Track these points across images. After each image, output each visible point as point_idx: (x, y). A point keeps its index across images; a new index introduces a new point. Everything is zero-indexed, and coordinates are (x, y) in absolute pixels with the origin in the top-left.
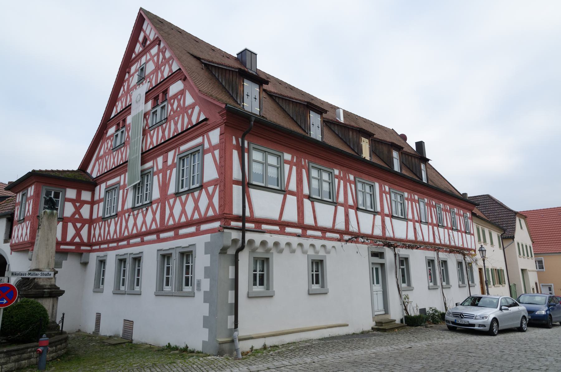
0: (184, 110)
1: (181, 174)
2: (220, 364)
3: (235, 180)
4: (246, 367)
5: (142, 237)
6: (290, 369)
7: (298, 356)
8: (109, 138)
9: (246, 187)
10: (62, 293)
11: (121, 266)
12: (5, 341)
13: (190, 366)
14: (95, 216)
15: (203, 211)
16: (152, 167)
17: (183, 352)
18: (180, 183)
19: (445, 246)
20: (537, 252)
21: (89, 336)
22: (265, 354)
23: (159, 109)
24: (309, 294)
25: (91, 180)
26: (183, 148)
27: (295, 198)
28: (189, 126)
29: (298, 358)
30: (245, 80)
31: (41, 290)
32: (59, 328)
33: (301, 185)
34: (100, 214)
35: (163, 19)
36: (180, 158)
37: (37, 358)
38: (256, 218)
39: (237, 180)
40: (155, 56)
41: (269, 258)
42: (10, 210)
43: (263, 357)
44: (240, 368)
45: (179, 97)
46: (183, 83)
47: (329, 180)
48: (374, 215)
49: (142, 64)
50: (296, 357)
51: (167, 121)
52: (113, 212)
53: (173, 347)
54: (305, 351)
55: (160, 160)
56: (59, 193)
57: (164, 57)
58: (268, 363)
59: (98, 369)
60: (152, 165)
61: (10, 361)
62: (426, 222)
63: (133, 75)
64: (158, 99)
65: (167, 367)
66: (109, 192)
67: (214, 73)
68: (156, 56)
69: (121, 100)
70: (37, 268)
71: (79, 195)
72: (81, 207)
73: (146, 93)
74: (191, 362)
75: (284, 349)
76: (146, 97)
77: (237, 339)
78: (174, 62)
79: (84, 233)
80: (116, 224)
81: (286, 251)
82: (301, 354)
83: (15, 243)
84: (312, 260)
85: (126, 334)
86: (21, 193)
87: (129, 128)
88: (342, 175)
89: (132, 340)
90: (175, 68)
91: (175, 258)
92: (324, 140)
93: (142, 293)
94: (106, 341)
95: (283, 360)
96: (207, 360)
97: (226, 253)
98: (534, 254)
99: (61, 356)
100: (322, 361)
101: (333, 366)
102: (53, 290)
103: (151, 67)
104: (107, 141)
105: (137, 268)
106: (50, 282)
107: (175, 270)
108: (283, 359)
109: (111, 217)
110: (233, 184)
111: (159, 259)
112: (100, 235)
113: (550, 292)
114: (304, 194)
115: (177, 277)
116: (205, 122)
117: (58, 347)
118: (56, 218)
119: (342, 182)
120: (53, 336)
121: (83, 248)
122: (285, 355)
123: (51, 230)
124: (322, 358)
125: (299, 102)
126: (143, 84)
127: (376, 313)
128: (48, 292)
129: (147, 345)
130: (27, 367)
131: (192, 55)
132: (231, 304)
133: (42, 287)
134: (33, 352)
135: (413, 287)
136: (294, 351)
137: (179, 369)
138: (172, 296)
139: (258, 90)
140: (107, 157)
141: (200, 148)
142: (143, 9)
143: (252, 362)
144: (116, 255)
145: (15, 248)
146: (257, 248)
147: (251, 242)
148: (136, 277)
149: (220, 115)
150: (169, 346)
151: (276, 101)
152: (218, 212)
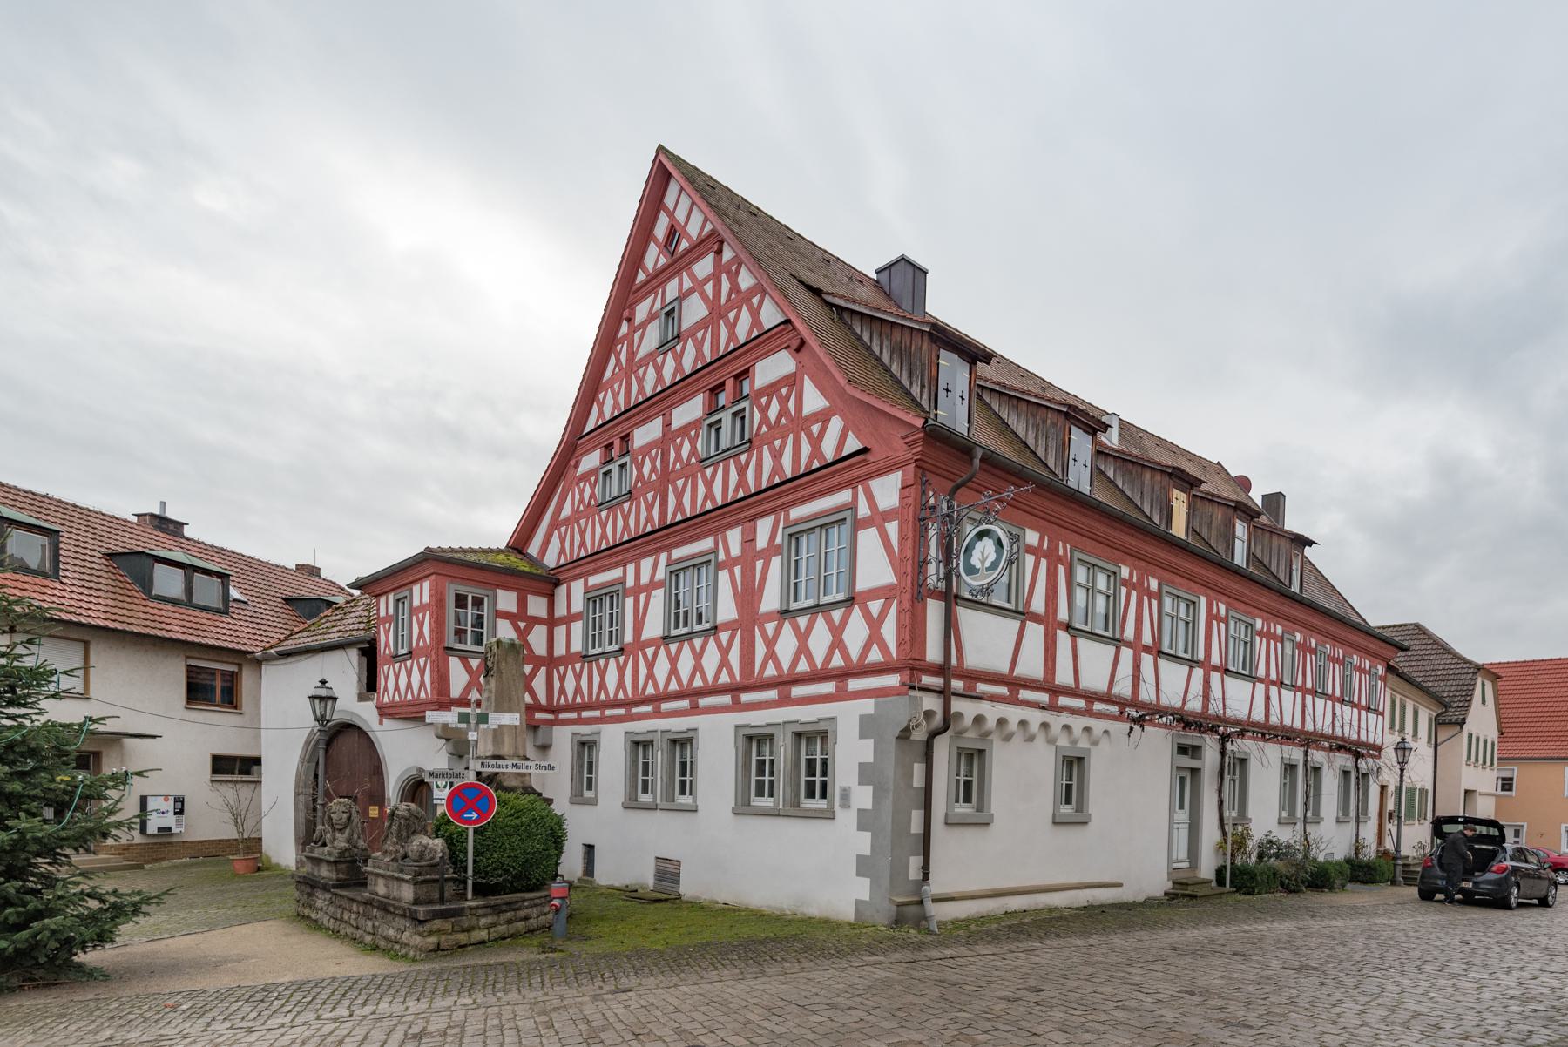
0: (800, 424)
11: (675, 754)
14: (560, 650)
18: (791, 589)
19: (1327, 737)
20: (1505, 756)
26: (796, 513)
27: (1040, 628)
40: (706, 281)
41: (984, 750)
45: (784, 391)
46: (795, 359)
47: (1108, 588)
48: (1191, 667)
52: (403, 648)
55: (734, 537)
57: (735, 287)
62: (1292, 686)
69: (612, 387)
70: (497, 753)
71: (522, 604)
72: (528, 630)
78: (767, 301)
81: (1018, 740)
90: (770, 316)
98: (1499, 759)
103: (695, 310)
104: (578, 484)
113: (1517, 839)
116: (861, 457)
119: (1134, 594)
121: (538, 716)
127: (1175, 866)
135: (1322, 819)
138: (779, 816)
141: (847, 514)
146: (965, 730)
152: (894, 655)
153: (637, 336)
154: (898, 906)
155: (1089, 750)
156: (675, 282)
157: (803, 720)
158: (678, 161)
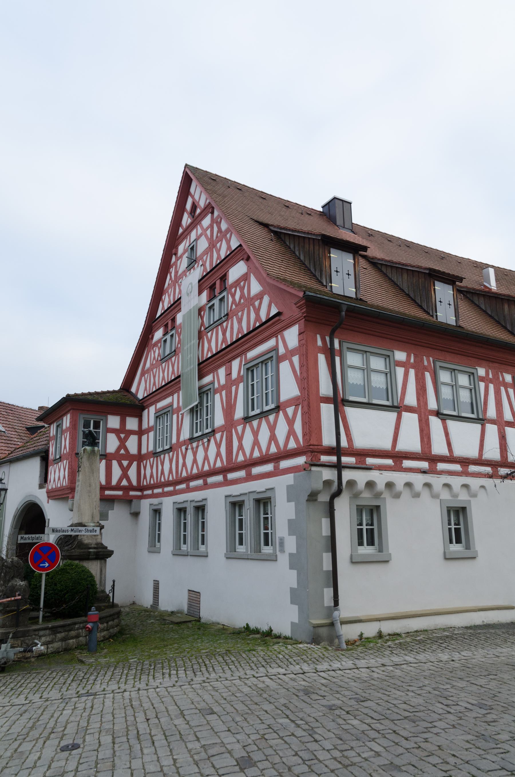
1: (250, 390)
2: (316, 656)
3: (323, 397)
4: (352, 662)
5: (205, 478)
6: (414, 667)
7: (430, 651)
8: (156, 345)
9: (340, 405)
10: (110, 554)
12: (49, 614)
13: (274, 656)
14: (144, 451)
15: (281, 442)
16: (213, 383)
17: (266, 637)
18: (250, 404)
21: (146, 610)
22: (380, 645)
23: (216, 302)
24: (446, 559)
25: (137, 402)
26: (251, 354)
27: (415, 416)
28: (258, 324)
29: (428, 653)
30: (332, 250)
31: (86, 550)
32: (110, 600)
33: (425, 397)
34: (151, 448)
35: (216, 175)
36: (248, 369)
37: (86, 636)
38: (356, 449)
39: (327, 396)
40: (207, 228)
41: (379, 506)
42: (43, 446)
43: (376, 649)
44: (342, 662)
45: (242, 284)
46: (246, 265)
47: (470, 385)
49: (192, 241)
50: (426, 652)
51: (227, 318)
52: (167, 445)
53: (253, 630)
54: (441, 643)
55: (222, 372)
56: (100, 422)
58: (384, 658)
59: (158, 654)
60: (212, 379)
61: (57, 640)
63: (181, 257)
64: (215, 288)
65: (244, 655)
66: (160, 418)
67: (288, 244)
68: (209, 229)
70: (80, 521)
71: (123, 423)
72: (126, 438)
73: (199, 281)
74: (275, 650)
75: (408, 640)
76: (199, 286)
77: (339, 621)
79: (132, 473)
80: (171, 461)
81: (406, 494)
82: (434, 647)
83: (52, 488)
84: (447, 507)
85: (192, 609)
86: (55, 424)
87: (179, 330)
88: (491, 376)
89: (200, 618)
90: (234, 244)
91: (249, 508)
92: (461, 323)
93: (209, 555)
94: (167, 618)
95: (406, 655)
96: (298, 649)
97: (316, 500)
99: (114, 635)
100: (466, 660)
101: (481, 668)
102: (100, 550)
103: (203, 245)
104: (153, 348)
105: (201, 520)
106: (96, 539)
107: (250, 523)
108: (406, 653)
109: (164, 451)
110: (321, 402)
111: (228, 508)
112: (152, 476)
114: (429, 408)
115: (252, 533)
117: (110, 623)
118: (98, 457)
119: (491, 387)
120: (103, 610)
121: (132, 493)
122: (409, 648)
123: (93, 473)
124: (466, 655)
125: (416, 269)
126: (194, 269)
128: (94, 552)
129: (219, 626)
130: (76, 648)
131: (256, 221)
132: (328, 571)
133: (87, 547)
134: (82, 629)
136: (423, 642)
137: (260, 659)
138: (248, 559)
139: (352, 261)
140: (155, 370)
141: (273, 354)
142: (189, 166)
143: (361, 655)
144: (174, 503)
145: (53, 495)
146: (361, 492)
147: (351, 483)
148: (200, 533)
149: (297, 307)
150: (247, 628)
151: (382, 271)
152: (302, 443)
153: (179, 262)
154: (314, 627)
155: (470, 501)
156: (195, 231)
157: (258, 490)
158: (195, 170)
